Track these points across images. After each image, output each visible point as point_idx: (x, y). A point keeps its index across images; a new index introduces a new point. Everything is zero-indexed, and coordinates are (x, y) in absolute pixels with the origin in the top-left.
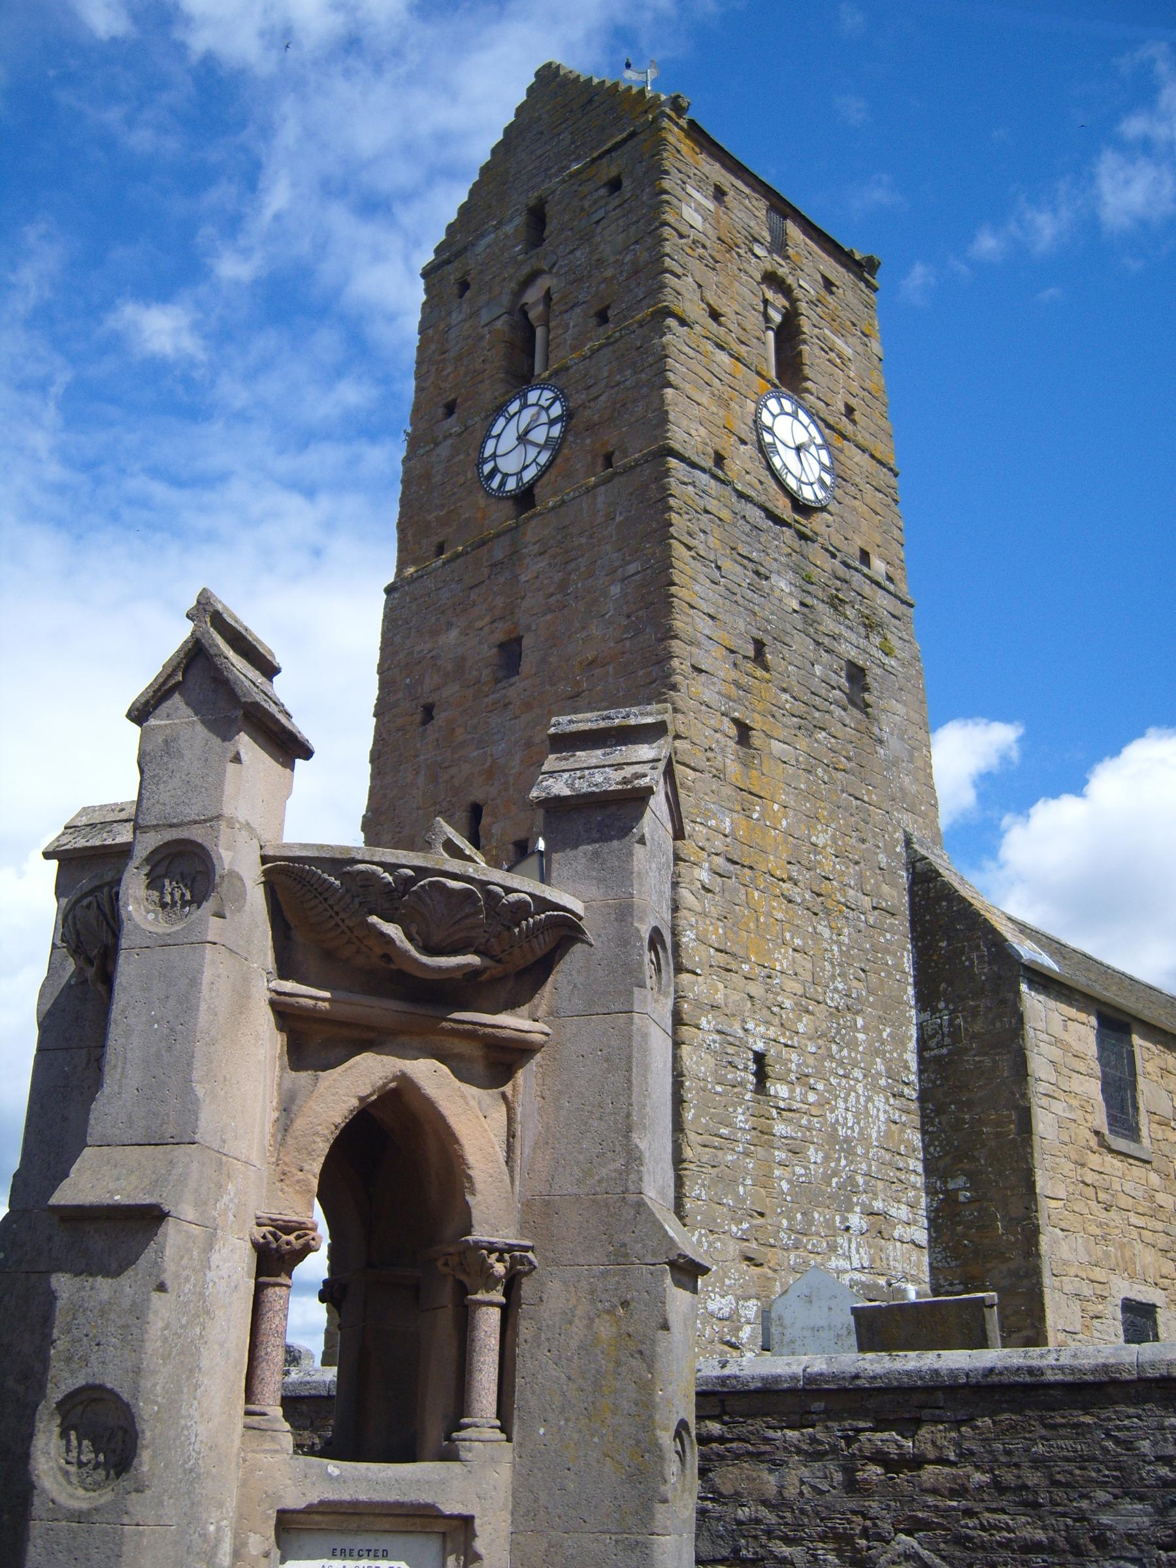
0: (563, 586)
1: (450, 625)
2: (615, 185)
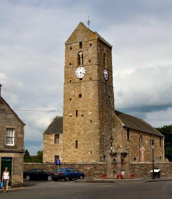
0: (86, 91)
1: (73, 91)
2: (91, 45)
